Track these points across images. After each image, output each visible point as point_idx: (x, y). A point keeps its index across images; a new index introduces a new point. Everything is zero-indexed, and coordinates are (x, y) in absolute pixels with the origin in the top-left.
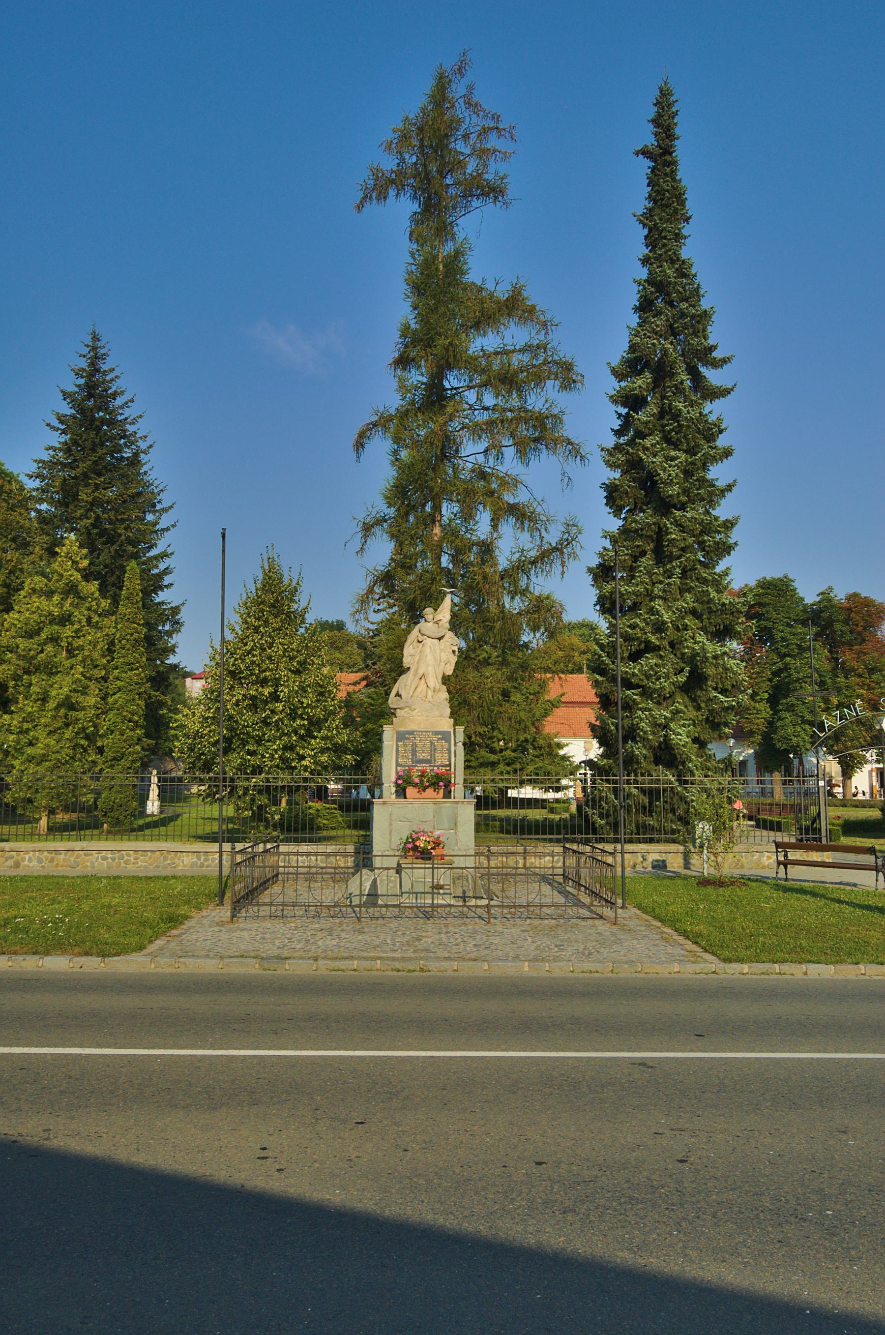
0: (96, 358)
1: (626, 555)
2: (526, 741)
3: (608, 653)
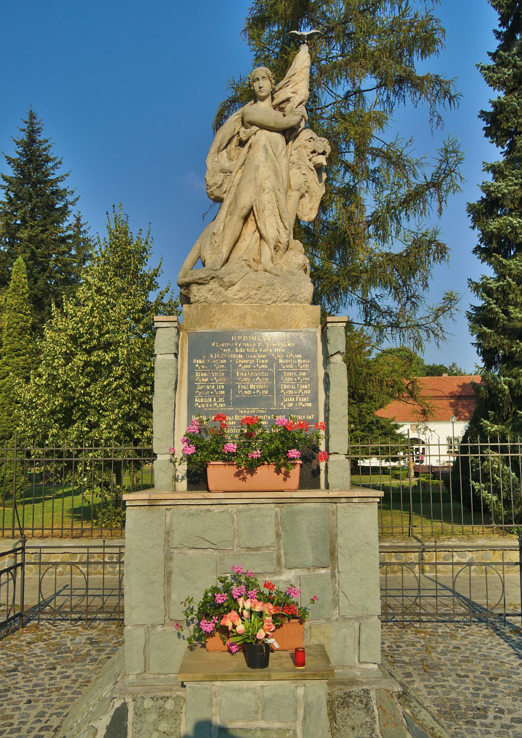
0: (32, 132)
1: (516, 184)
2: (372, 422)
3: (497, 299)
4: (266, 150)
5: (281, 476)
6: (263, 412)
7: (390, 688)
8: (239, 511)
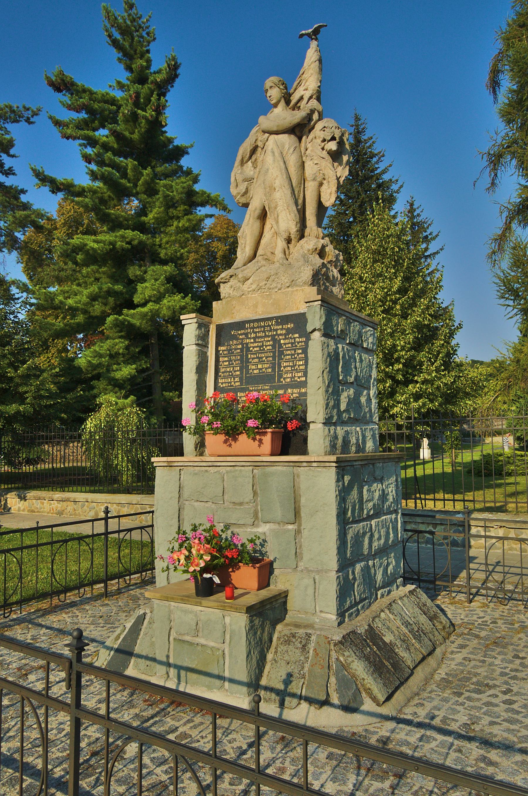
4: (273, 153)
5: (257, 442)
6: (267, 387)
7: (330, 636)
8: (227, 472)
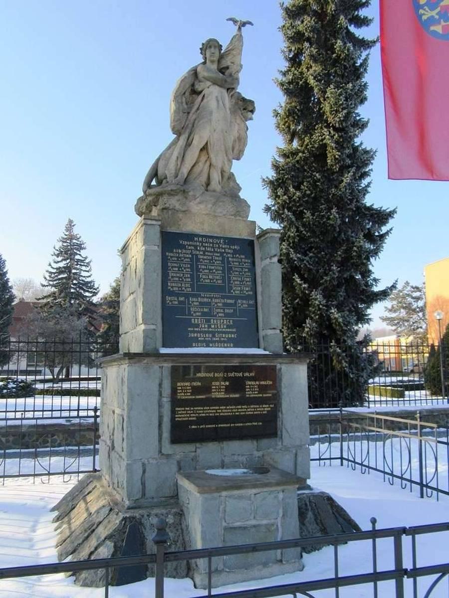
4: (218, 101)
